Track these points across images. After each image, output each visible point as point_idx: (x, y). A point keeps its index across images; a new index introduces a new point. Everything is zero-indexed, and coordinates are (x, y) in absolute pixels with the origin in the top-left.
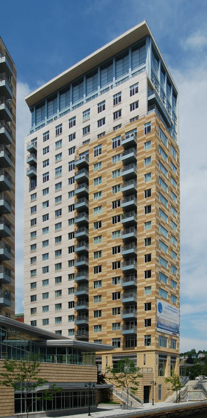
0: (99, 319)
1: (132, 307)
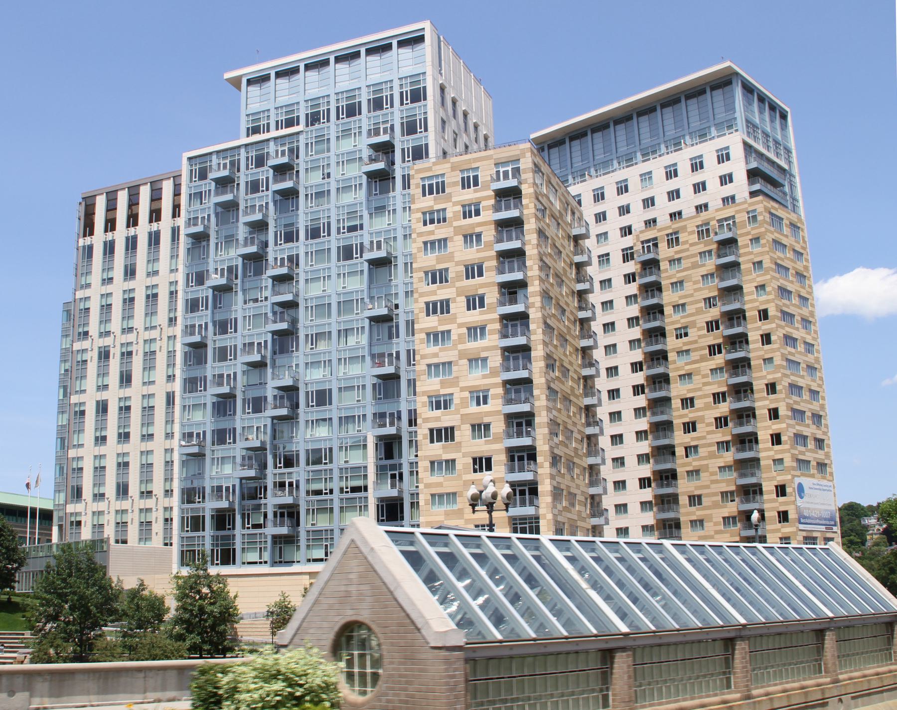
0: (698, 510)
1: (741, 342)
